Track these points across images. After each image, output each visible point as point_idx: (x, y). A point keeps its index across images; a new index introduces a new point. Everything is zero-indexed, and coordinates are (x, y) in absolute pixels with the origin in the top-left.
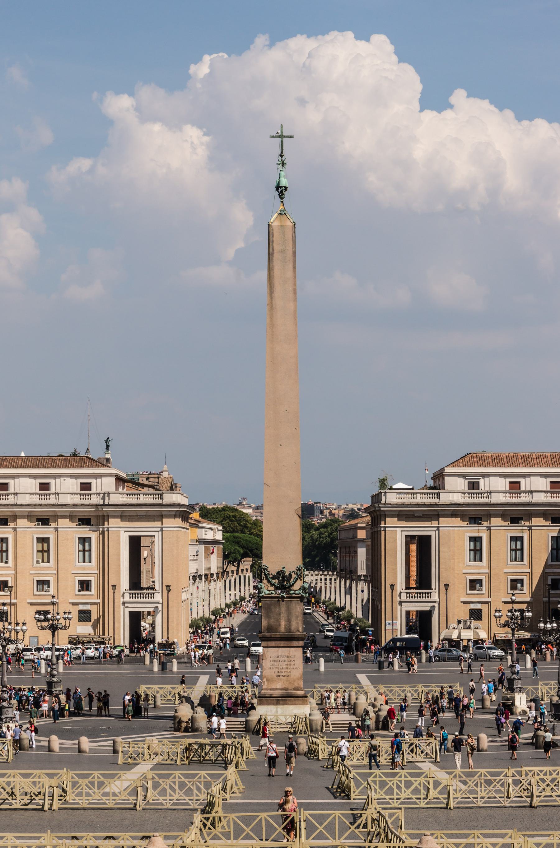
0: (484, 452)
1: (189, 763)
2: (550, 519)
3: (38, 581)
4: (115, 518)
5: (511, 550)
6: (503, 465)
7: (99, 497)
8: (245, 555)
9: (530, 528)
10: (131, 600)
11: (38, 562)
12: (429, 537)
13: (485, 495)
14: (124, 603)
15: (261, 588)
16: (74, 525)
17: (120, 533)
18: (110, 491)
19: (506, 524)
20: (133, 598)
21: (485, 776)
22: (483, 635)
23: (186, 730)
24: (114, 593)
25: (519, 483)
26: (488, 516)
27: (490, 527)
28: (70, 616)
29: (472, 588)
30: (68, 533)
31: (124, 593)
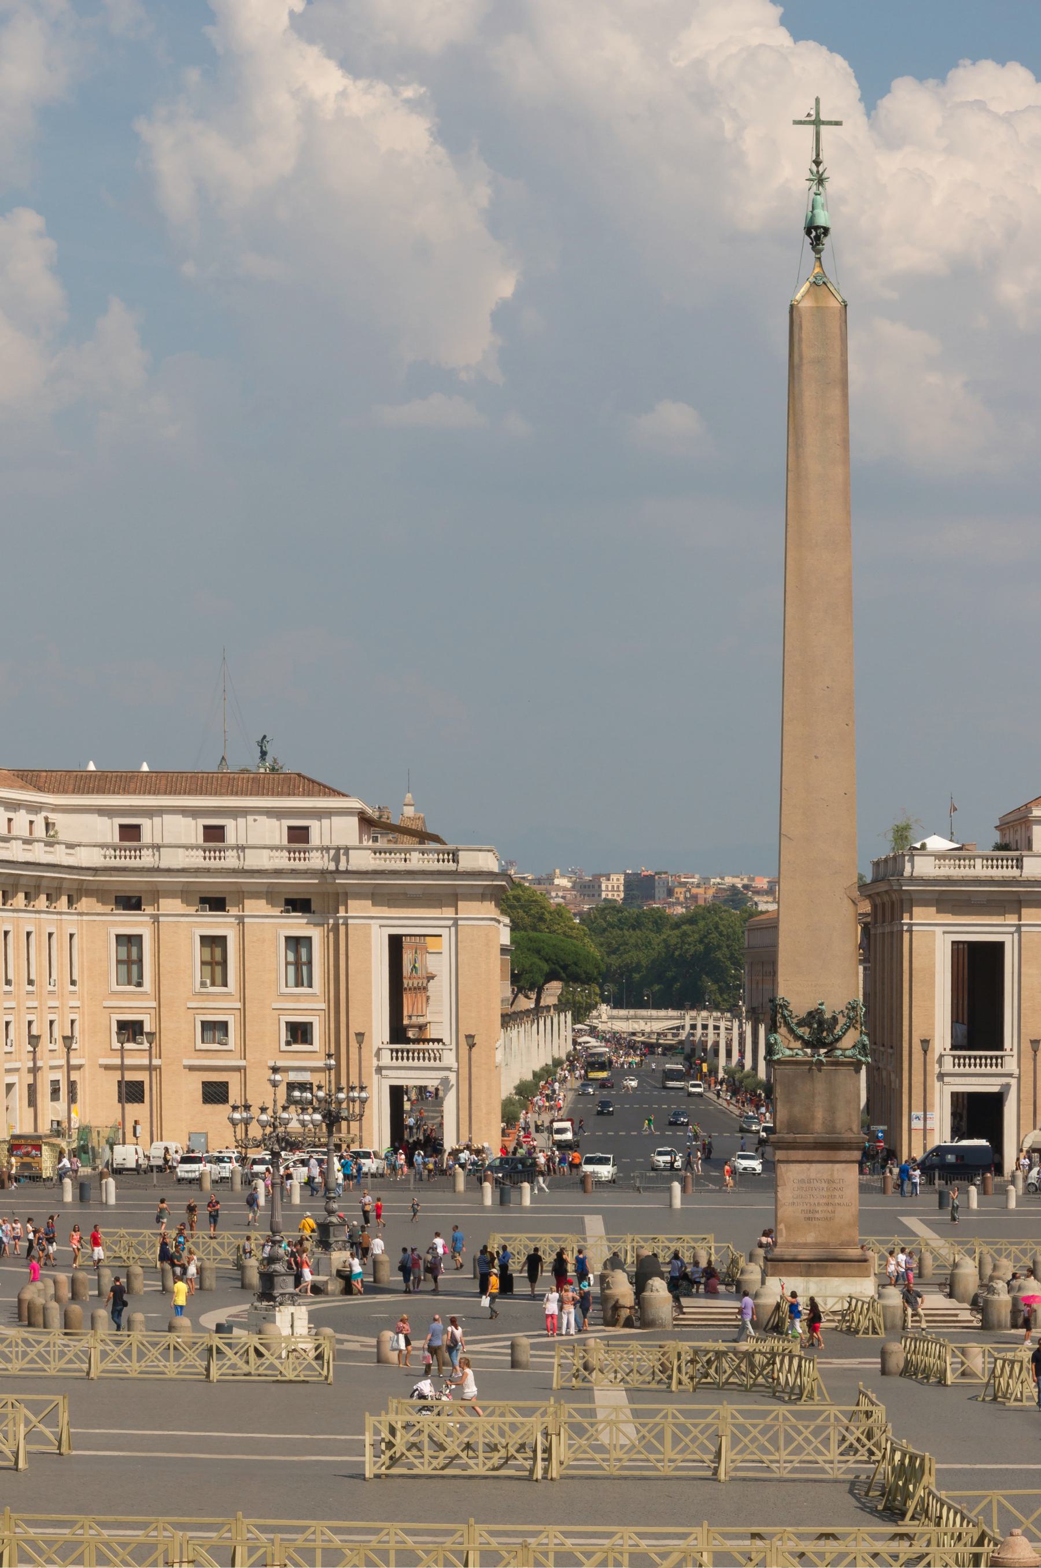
1: (694, 1390)
3: (203, 1022)
4: (360, 899)
7: (326, 855)
11: (203, 984)
12: (1001, 945)
14: (379, 1070)
15: (776, 1042)
16: (276, 911)
17: (371, 928)
18: (349, 844)
20: (397, 1059)
21: (674, 1417)
23: (628, 1323)
24: (360, 1048)
26: (241, 895)
28: (364, 1095)
30: (267, 927)
31: (379, 1049)
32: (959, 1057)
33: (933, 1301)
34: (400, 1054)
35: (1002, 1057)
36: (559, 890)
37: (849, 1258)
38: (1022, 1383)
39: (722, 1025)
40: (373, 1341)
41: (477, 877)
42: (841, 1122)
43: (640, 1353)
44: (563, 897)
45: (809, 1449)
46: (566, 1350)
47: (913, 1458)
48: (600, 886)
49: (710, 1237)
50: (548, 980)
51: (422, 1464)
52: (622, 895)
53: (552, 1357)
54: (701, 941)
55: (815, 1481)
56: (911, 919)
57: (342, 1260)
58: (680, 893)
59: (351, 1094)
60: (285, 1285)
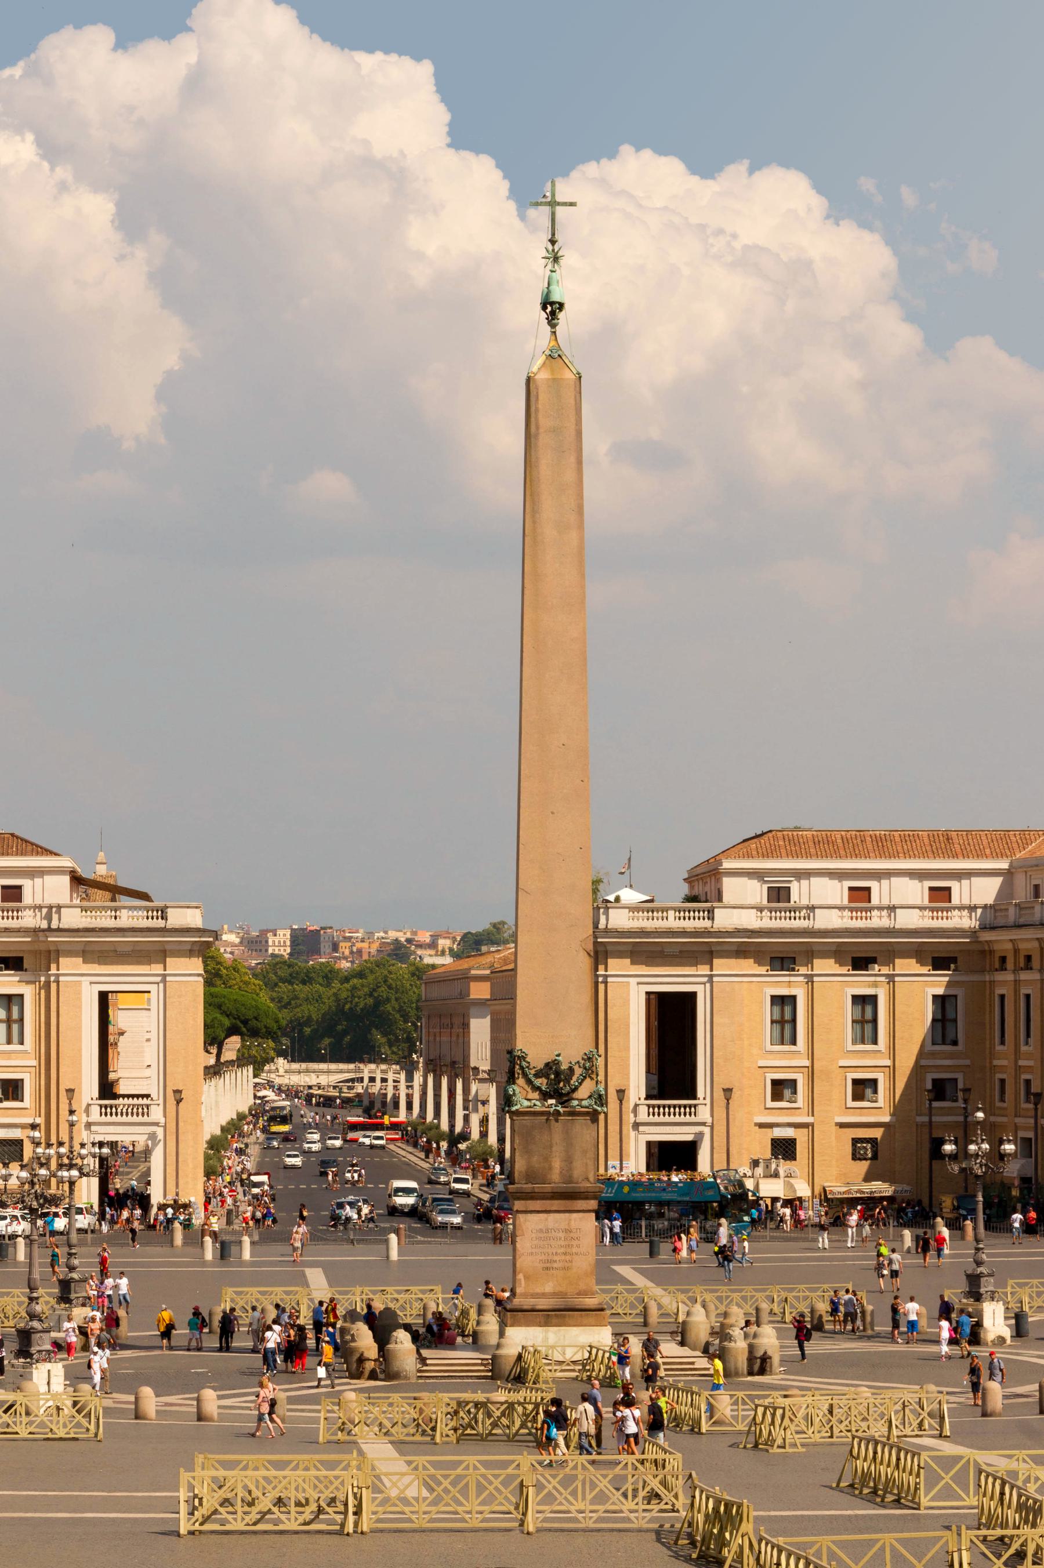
0: (797, 829)
1: (458, 1441)
2: (930, 961)
5: (853, 1021)
6: (836, 855)
7: (38, 914)
8: (232, 1031)
9: (891, 978)
10: (103, 1119)
12: (693, 996)
13: (802, 914)
14: (88, 1125)
15: (514, 1094)
17: (80, 984)
18: (61, 902)
19: (844, 970)
22: (803, 1190)
23: (373, 1376)
25: (949, 889)
26: (810, 954)
27: (812, 976)
29: (777, 1096)
31: (89, 1105)
32: (654, 1107)
33: (669, 1349)
34: (109, 1110)
35: (695, 1106)
36: (227, 946)
37: (587, 1307)
38: (785, 1429)
39: (391, 1077)
40: (132, 1398)
41: (187, 934)
42: (577, 1173)
43: (398, 1407)
44: (232, 953)
45: (447, 1498)
46: (333, 1404)
47: (728, 1506)
48: (267, 942)
49: (438, 1288)
50: (227, 1036)
51: (235, 1519)
52: (288, 950)
53: (319, 1411)
54: (371, 995)
55: (620, 1530)
56: (606, 970)
57: (83, 1316)
58: (345, 948)
59: (47, 1151)
60: (42, 1343)
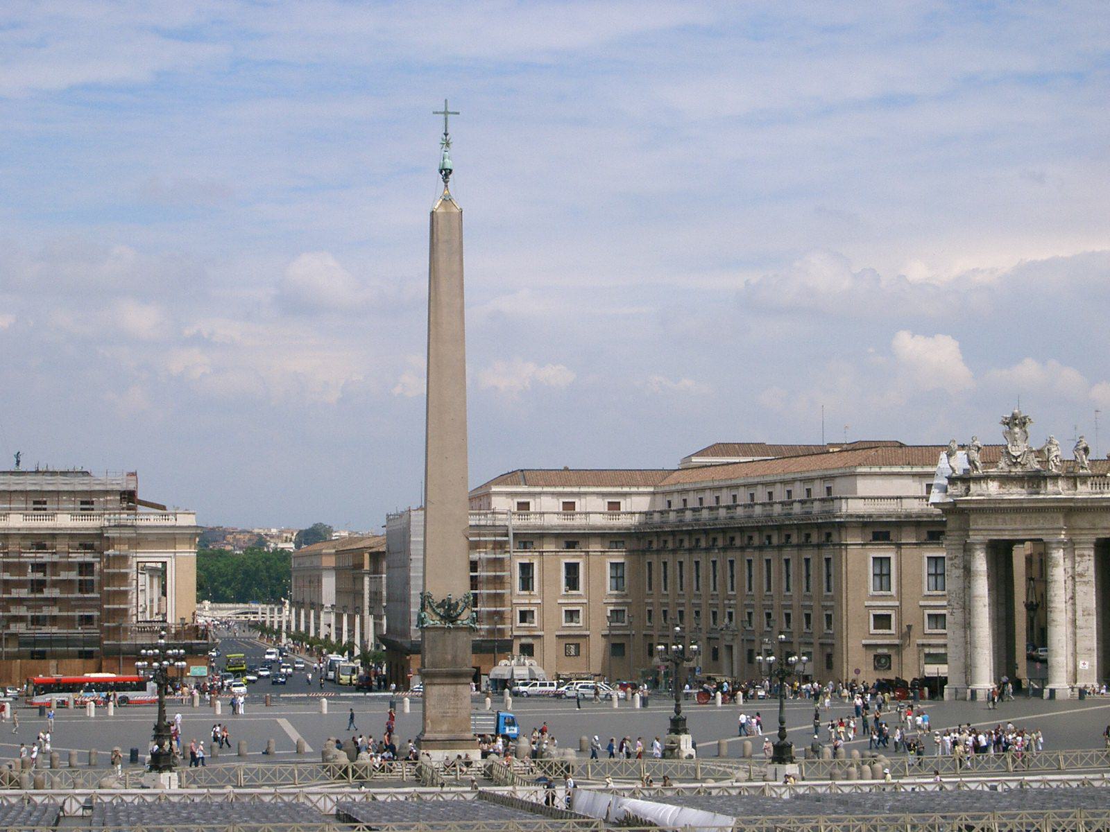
5: (611, 577)
